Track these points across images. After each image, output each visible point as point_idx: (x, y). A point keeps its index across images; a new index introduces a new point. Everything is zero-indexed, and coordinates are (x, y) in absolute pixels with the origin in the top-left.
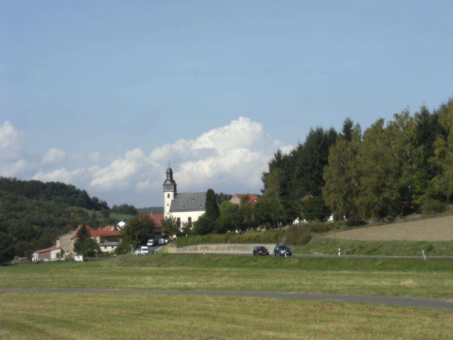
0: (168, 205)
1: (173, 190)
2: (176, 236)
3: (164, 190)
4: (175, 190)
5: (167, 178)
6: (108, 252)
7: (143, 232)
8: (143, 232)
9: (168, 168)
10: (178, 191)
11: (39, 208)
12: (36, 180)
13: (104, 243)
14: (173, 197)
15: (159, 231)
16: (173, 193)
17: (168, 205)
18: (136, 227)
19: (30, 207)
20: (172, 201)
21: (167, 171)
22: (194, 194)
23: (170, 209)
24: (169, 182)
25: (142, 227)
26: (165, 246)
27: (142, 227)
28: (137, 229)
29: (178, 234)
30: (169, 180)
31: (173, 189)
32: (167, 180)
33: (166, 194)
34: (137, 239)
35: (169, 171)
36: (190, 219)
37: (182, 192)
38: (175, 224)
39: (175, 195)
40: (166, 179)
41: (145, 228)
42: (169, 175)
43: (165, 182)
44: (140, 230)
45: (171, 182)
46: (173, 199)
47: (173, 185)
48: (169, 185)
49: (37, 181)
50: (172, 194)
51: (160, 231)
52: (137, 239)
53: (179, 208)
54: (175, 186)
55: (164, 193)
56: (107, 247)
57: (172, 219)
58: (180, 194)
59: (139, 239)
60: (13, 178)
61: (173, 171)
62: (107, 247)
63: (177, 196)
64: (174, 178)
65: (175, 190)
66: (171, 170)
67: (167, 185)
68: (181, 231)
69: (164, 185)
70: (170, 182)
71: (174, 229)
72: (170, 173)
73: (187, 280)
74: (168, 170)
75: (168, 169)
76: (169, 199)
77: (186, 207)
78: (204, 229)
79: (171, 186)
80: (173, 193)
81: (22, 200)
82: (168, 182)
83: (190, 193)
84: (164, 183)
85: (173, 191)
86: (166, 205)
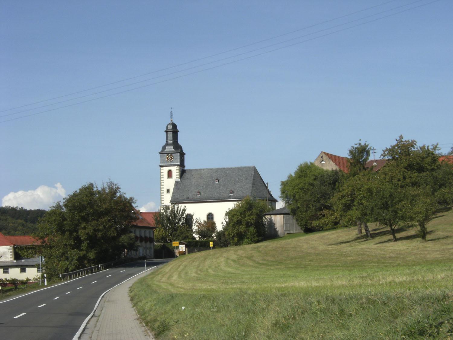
0: (168, 191)
1: (179, 163)
2: (186, 247)
3: (160, 163)
4: (182, 165)
5: (167, 141)
6: (28, 280)
7: (101, 228)
8: (101, 228)
9: (169, 121)
10: (188, 166)
11: (22, 228)
12: (41, 209)
13: (23, 261)
14: (178, 176)
15: (148, 235)
16: (178, 168)
17: (168, 191)
18: (83, 214)
19: (13, 227)
20: (176, 183)
21: (167, 127)
22: (217, 170)
23: (172, 197)
24: (170, 148)
25: (99, 215)
26: (160, 266)
27: (99, 215)
28: (85, 219)
29: (189, 242)
30: (170, 145)
31: (179, 160)
32: (167, 144)
33: (165, 170)
34: (85, 245)
35: (170, 127)
36: (210, 216)
37: (194, 168)
38: (182, 223)
39: (183, 173)
40: (164, 143)
41: (107, 218)
42: (170, 135)
43: (164, 148)
44: (94, 223)
45: (174, 148)
46: (179, 180)
47: (179, 154)
48: (171, 153)
49: (42, 210)
50: (175, 170)
51: (152, 236)
52: (85, 245)
53: (190, 196)
54: (182, 155)
55: (162, 169)
56: (28, 269)
57: (177, 210)
58: (191, 170)
59: (91, 246)
60: (20, 208)
61: (178, 129)
62: (28, 269)
63: (186, 175)
64: (180, 142)
65: (182, 165)
66: (174, 126)
67: (167, 153)
68: (197, 237)
69: (161, 153)
70: (172, 147)
71: (182, 233)
72: (174, 131)
73: (186, 303)
74: (169, 126)
75: (169, 124)
76: (170, 179)
77: (202, 193)
78: (251, 226)
79: (173, 154)
80: (178, 168)
81: (6, 220)
82: (168, 149)
83: (211, 169)
84: (160, 150)
85: (177, 165)
86: (165, 191)
